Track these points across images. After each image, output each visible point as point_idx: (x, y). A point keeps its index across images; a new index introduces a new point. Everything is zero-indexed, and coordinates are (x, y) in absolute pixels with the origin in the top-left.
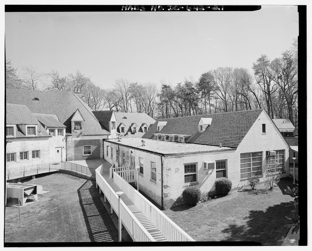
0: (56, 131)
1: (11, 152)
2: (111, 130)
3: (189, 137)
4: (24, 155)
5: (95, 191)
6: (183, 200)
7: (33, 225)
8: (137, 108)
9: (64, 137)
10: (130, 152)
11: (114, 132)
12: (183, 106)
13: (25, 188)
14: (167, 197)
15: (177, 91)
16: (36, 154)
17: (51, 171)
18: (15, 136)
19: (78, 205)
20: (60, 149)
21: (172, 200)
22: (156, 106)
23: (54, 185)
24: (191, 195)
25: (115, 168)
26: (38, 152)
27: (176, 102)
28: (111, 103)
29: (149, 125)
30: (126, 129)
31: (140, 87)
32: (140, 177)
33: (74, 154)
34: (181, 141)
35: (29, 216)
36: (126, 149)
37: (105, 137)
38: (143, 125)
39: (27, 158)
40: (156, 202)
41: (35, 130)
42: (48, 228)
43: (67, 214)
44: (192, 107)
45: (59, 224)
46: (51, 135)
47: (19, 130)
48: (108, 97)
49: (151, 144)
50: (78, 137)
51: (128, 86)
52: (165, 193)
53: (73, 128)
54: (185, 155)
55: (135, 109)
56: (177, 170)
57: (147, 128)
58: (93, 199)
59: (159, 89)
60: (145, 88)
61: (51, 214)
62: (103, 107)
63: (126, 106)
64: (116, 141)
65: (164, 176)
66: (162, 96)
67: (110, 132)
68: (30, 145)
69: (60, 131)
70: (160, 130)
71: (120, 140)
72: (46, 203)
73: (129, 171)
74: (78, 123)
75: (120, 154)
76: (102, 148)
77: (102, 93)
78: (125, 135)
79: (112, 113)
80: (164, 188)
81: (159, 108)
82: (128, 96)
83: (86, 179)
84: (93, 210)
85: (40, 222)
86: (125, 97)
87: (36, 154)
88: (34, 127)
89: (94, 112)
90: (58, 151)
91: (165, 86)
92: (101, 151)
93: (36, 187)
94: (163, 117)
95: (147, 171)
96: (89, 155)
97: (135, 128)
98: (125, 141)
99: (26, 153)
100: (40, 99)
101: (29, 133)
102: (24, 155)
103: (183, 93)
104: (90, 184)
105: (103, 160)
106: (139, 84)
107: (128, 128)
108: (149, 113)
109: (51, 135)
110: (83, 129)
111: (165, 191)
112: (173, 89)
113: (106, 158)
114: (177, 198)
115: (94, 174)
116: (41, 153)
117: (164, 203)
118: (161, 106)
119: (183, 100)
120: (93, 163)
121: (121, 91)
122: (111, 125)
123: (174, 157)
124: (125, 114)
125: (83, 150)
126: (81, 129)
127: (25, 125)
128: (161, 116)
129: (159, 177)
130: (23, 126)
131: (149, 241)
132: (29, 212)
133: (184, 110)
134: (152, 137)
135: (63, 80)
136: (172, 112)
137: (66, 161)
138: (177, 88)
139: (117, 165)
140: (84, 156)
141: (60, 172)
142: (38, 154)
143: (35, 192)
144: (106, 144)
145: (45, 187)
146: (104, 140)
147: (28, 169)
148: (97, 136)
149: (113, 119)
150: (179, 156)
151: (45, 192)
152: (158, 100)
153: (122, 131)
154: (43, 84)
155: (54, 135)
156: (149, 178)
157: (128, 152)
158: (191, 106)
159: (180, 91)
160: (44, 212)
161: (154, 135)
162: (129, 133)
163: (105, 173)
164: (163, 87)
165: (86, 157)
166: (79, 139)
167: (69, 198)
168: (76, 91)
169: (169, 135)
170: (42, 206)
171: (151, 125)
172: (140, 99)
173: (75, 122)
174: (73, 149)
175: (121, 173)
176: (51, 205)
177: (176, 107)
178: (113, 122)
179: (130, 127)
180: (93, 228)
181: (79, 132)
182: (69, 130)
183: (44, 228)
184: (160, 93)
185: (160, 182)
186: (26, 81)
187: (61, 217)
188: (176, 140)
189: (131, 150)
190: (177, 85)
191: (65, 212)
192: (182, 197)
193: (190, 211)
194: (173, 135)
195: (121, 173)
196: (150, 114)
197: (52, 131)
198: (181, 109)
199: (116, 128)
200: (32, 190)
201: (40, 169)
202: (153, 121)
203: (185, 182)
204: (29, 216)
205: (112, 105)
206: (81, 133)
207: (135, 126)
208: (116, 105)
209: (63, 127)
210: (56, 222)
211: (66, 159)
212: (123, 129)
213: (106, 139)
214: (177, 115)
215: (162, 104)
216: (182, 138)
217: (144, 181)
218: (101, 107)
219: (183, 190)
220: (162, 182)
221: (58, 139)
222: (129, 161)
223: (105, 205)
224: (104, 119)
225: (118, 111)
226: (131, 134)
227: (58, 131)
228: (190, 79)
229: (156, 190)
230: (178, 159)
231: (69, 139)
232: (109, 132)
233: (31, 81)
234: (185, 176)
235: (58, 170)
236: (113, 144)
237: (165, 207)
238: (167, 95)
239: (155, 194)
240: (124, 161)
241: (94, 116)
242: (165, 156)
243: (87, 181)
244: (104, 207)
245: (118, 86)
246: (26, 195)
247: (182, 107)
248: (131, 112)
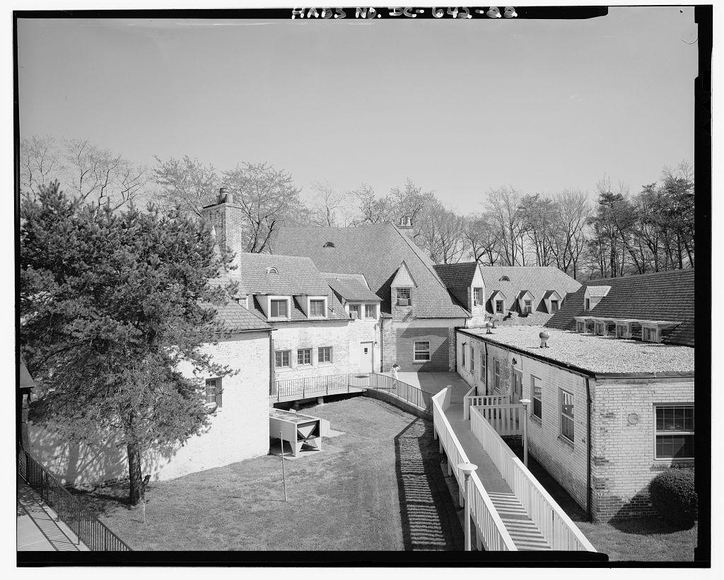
0: (363, 308)
1: (284, 349)
2: (473, 308)
3: (674, 328)
4: (305, 356)
5: (430, 445)
6: (650, 505)
7: (306, 501)
8: (538, 254)
9: (377, 321)
10: (511, 361)
11: (478, 311)
12: (661, 245)
13: (299, 423)
14: (604, 488)
15: (642, 207)
16: (325, 354)
17: (352, 391)
18: (290, 318)
19: (392, 472)
20: (369, 346)
21: (617, 499)
22: (586, 249)
23: (353, 421)
24: (677, 495)
25: (477, 397)
26: (328, 349)
27: (639, 234)
28: (478, 245)
29: (563, 295)
30: (507, 306)
31: (546, 204)
32: (533, 425)
33: (395, 358)
34: (649, 338)
35: (302, 481)
36: (501, 353)
37: (459, 323)
38: (548, 294)
39: (309, 362)
40: (573, 496)
41: (323, 305)
42: (331, 513)
43: (369, 488)
44: (687, 247)
45: (353, 508)
46: (353, 318)
47: (297, 306)
48: (472, 234)
49: (565, 344)
50: (404, 320)
51: (516, 204)
52: (597, 477)
53: (394, 303)
54: (659, 380)
55: (532, 256)
56: (634, 419)
57: (560, 303)
58: (425, 462)
59: (592, 204)
60: (556, 206)
61: (341, 484)
62: (460, 255)
63: (510, 252)
64: (482, 333)
65: (596, 432)
66: (598, 222)
67: (470, 311)
68: (316, 336)
69: (370, 308)
70: (593, 305)
71: (492, 330)
72: (335, 458)
73: (509, 406)
74: (405, 292)
75: (489, 363)
76: (453, 348)
77: (458, 224)
78: (505, 319)
79: (474, 269)
80: (596, 464)
81: (591, 252)
82: (517, 228)
83: (415, 415)
84: (420, 490)
85: (320, 498)
86: (508, 231)
87: (325, 354)
88: (322, 301)
89: (436, 268)
90: (366, 350)
91: (608, 198)
92: (452, 355)
93: (318, 422)
94: (603, 273)
95: (551, 411)
96: (425, 361)
97: (528, 303)
98: (503, 334)
99: (308, 351)
100: (336, 245)
101: (314, 313)
102: (305, 356)
103: (658, 211)
104: (420, 429)
105: (454, 374)
106: (542, 198)
107: (512, 302)
108: (566, 265)
109: (353, 318)
110: (414, 305)
111: (597, 473)
112: (632, 203)
113: (461, 371)
114: (632, 497)
115: (430, 405)
116: (335, 353)
117: (594, 505)
118: (599, 247)
119: (659, 228)
120: (432, 379)
121: (501, 218)
122: (473, 296)
123: (624, 383)
124: (507, 270)
125: (414, 351)
126: (410, 304)
127: (307, 296)
128: (597, 274)
129: (580, 432)
130: (304, 298)
131: (580, 549)
132: (303, 472)
133: (662, 255)
134: (570, 326)
135: (381, 205)
136: (629, 262)
137: (382, 371)
138: (643, 197)
139: (482, 389)
140: (416, 364)
141: (368, 394)
142: (329, 355)
143: (316, 433)
144: (461, 338)
145: (336, 423)
146: (457, 329)
147: (312, 384)
148: (442, 320)
149: (477, 281)
150: (640, 380)
151: (337, 434)
152: (589, 233)
153: (498, 310)
154: (347, 213)
155: (359, 317)
156: (556, 430)
157: (506, 361)
158: (683, 245)
159: (651, 207)
160: (330, 476)
161: (574, 321)
162: (515, 314)
163: (454, 407)
164: (602, 199)
165: (420, 366)
166: (405, 326)
167: (379, 453)
168: (402, 225)
169: (615, 321)
170: (327, 464)
171: (569, 296)
172: (543, 233)
173: (475, 288)
174: (394, 347)
175: (490, 410)
176: (343, 464)
177: (639, 248)
178: (477, 290)
179: (543, 300)
180: (415, 532)
181: (405, 310)
182: (386, 307)
183: (324, 513)
184: (595, 215)
185: (584, 447)
186: (316, 211)
187: (358, 494)
188: (637, 335)
189: (513, 355)
190: (642, 189)
191: (366, 485)
192: (647, 494)
193: (674, 541)
194: (627, 321)
195: (490, 410)
196: (569, 269)
197: (355, 308)
198: (655, 252)
199: (485, 301)
200: (311, 428)
201: (332, 385)
202: (574, 286)
203: (659, 454)
204: (302, 481)
205: (480, 249)
206: (409, 314)
207: (555, 299)
208: (489, 250)
209: (375, 301)
210: (348, 504)
211: (382, 367)
212: (500, 304)
213: (460, 328)
214: (642, 269)
215: (600, 242)
216: (654, 330)
217: (544, 436)
218: (457, 256)
219: (654, 474)
220: (590, 447)
221: (366, 326)
222: (510, 381)
223: (448, 482)
224: (457, 283)
225: (492, 263)
226: (519, 316)
227: (366, 308)
228: (681, 171)
229: (572, 465)
230: (635, 390)
231: (387, 324)
232: (468, 313)
233: (325, 210)
234: (658, 437)
235: (364, 391)
236: (475, 341)
237: (598, 516)
238: (613, 220)
239: (570, 474)
240: (497, 383)
241: (437, 276)
242: (596, 379)
243: (415, 421)
244: (446, 486)
245: (493, 206)
246: (300, 437)
247: (656, 247)
248: (522, 264)
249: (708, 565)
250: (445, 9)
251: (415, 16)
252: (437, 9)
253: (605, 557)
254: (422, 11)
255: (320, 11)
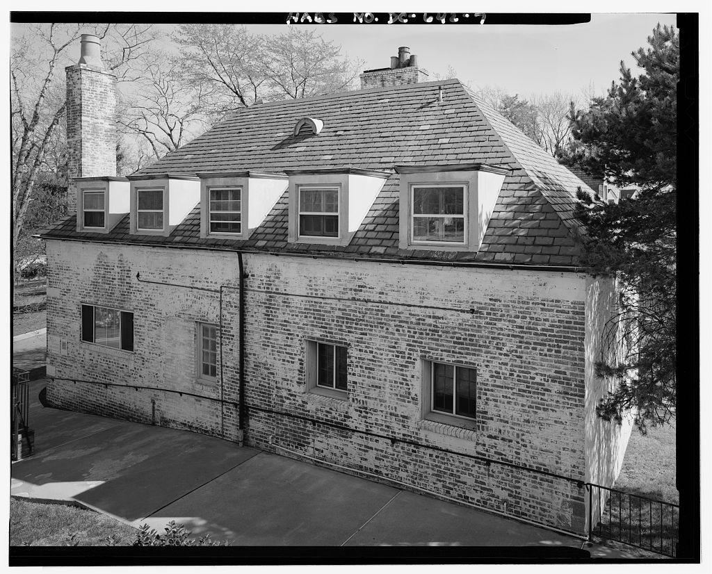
59: (673, 21)
249: (695, 558)
250: (434, 15)
251: (406, 21)
252: (429, 15)
253: (588, 553)
254: (414, 16)
255: (312, 15)
